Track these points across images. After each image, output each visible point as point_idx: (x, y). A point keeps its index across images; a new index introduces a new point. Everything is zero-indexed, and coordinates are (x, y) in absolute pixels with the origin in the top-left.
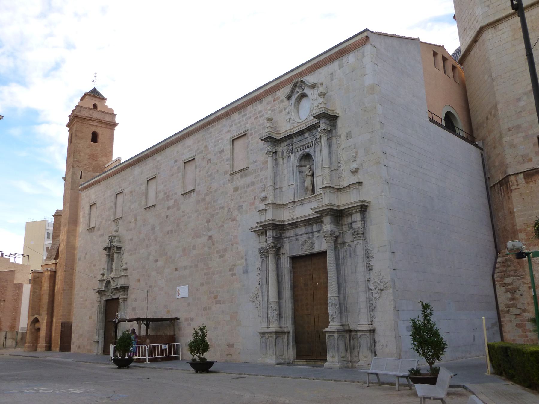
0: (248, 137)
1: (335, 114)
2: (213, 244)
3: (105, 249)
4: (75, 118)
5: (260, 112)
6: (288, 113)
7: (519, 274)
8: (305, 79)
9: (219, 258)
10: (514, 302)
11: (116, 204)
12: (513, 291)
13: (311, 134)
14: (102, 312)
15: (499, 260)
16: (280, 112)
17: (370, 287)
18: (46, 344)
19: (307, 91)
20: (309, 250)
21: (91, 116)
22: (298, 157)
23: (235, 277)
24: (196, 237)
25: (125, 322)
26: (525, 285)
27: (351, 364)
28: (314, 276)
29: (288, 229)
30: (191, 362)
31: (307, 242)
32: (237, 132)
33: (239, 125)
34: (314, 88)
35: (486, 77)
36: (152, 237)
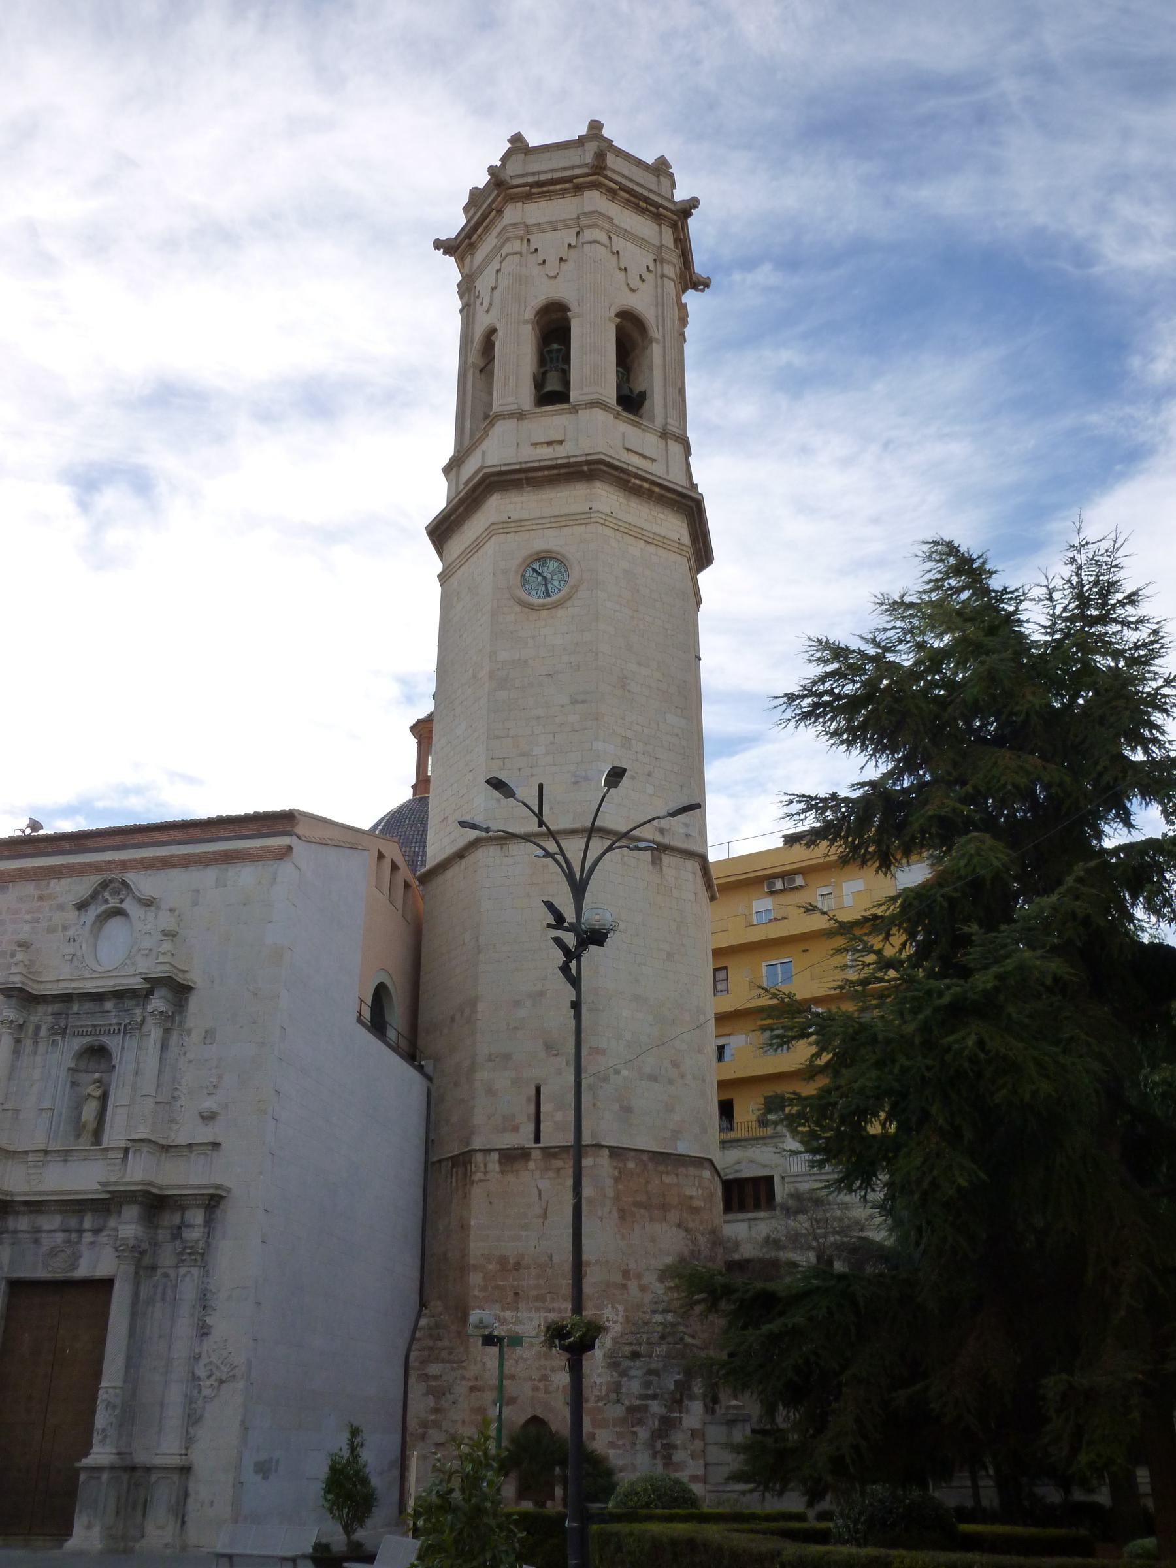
1: (190, 984)
6: (71, 940)
7: (456, 1358)
8: (130, 877)
12: (439, 1393)
13: (121, 1005)
15: (423, 1322)
16: (51, 930)
19: (128, 905)
22: (77, 1048)
26: (464, 1383)
29: (17, 1213)
31: (63, 1251)
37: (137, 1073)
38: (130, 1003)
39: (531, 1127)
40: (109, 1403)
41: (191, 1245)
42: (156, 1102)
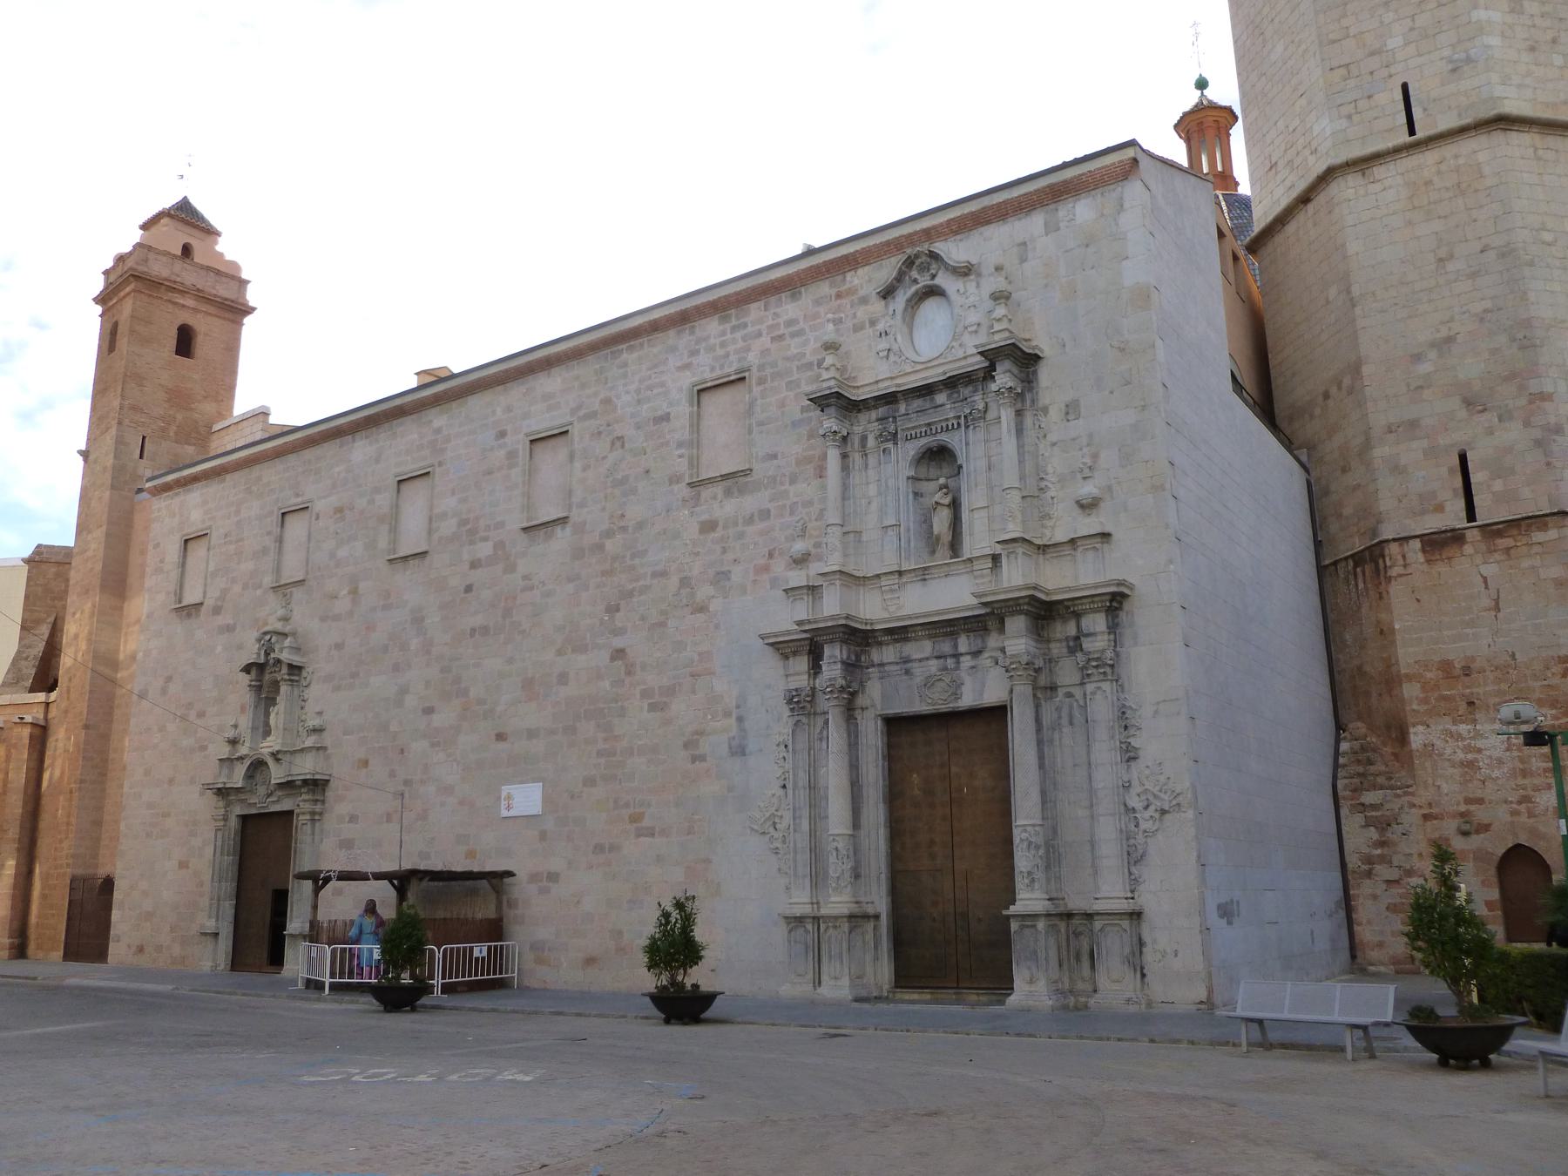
0: (750, 386)
2: (629, 673)
3: (247, 669)
4: (131, 279)
5: (790, 323)
8: (940, 247)
9: (649, 711)
10: (1386, 851)
11: (280, 540)
12: (1384, 825)
13: (956, 395)
14: (232, 850)
15: (1344, 746)
16: (858, 328)
17: (1131, 804)
18: (11, 940)
19: (942, 280)
20: (945, 700)
21: (178, 279)
23: (704, 764)
24: (570, 650)
25: (369, 879)
26: (1413, 810)
27: (1072, 998)
28: (954, 769)
29: (880, 644)
30: (653, 993)
32: (713, 369)
33: (720, 352)
34: (966, 275)
35: (1333, 292)
36: (415, 644)
37: (990, 469)
38: (965, 391)
39: (1461, 504)
40: (1030, 843)
41: (1096, 656)
42: (1023, 497)
